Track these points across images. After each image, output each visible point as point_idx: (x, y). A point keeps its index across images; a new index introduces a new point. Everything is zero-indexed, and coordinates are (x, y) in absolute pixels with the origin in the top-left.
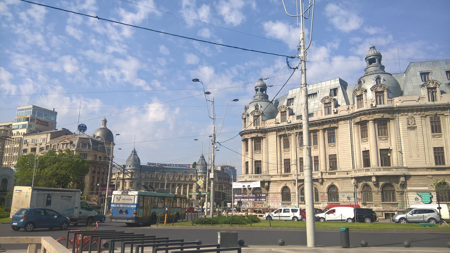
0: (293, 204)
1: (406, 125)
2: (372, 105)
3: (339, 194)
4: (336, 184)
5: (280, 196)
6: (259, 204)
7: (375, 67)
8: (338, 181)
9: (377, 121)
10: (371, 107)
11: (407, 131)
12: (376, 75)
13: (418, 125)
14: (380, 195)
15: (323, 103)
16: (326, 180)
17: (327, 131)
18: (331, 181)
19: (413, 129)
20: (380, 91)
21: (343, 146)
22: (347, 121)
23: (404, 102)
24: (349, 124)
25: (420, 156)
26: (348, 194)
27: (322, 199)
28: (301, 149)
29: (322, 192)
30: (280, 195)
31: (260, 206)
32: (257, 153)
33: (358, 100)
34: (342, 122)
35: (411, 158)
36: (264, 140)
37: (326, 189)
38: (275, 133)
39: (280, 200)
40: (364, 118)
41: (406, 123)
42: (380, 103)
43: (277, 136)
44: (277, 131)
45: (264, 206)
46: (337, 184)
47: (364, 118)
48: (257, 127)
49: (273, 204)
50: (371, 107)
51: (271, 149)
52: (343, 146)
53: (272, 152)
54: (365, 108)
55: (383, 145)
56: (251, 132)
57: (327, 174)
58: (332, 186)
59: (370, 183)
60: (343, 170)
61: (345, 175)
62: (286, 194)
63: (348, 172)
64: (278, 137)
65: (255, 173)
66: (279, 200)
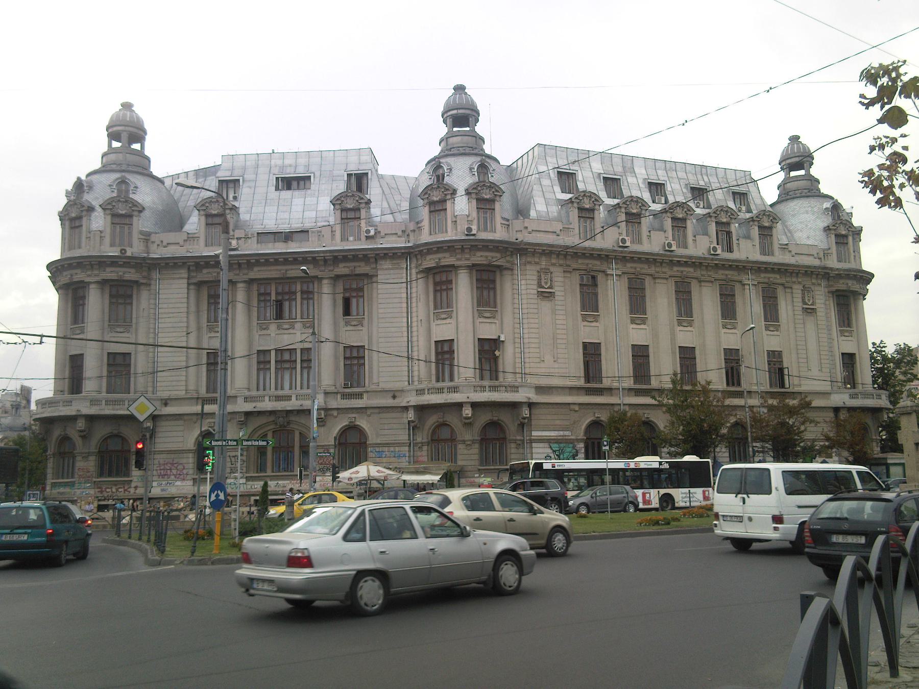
0: (232, 481)
1: (535, 287)
2: (469, 229)
3: (369, 449)
4: (363, 423)
5: (191, 460)
6: (116, 485)
7: (470, 137)
8: (369, 416)
9: (111, 286)
10: (467, 235)
11: (536, 301)
12: (118, 175)
13: (558, 290)
14: (475, 449)
15: (108, 212)
16: (335, 413)
17: (255, 287)
18: (350, 415)
19: (548, 297)
20: (437, 201)
21: (387, 325)
22: (399, 262)
23: (534, 234)
24: (405, 270)
25: (559, 361)
26: (392, 449)
27: (321, 464)
28: (265, 327)
29: (323, 446)
30: (191, 455)
31: (120, 490)
32: (118, 330)
33: (433, 211)
34: (386, 264)
35: (542, 365)
36: (144, 294)
37: (583, 427)
38: (184, 273)
39: (191, 472)
40: (448, 260)
41: (536, 282)
42: (485, 230)
43: (189, 284)
44: (191, 268)
45: (132, 490)
46: (365, 422)
47: (79, 276)
48: (123, 251)
49: (164, 483)
50: (467, 235)
51: (168, 320)
52: (387, 325)
53: (172, 330)
54: (451, 235)
55: (488, 331)
56: (102, 262)
57: (339, 396)
58: (352, 428)
59: (73, 433)
60: (383, 386)
61: (388, 402)
62: (593, 443)
63: (397, 394)
64: (192, 287)
65: (108, 393)
66: (185, 472)
